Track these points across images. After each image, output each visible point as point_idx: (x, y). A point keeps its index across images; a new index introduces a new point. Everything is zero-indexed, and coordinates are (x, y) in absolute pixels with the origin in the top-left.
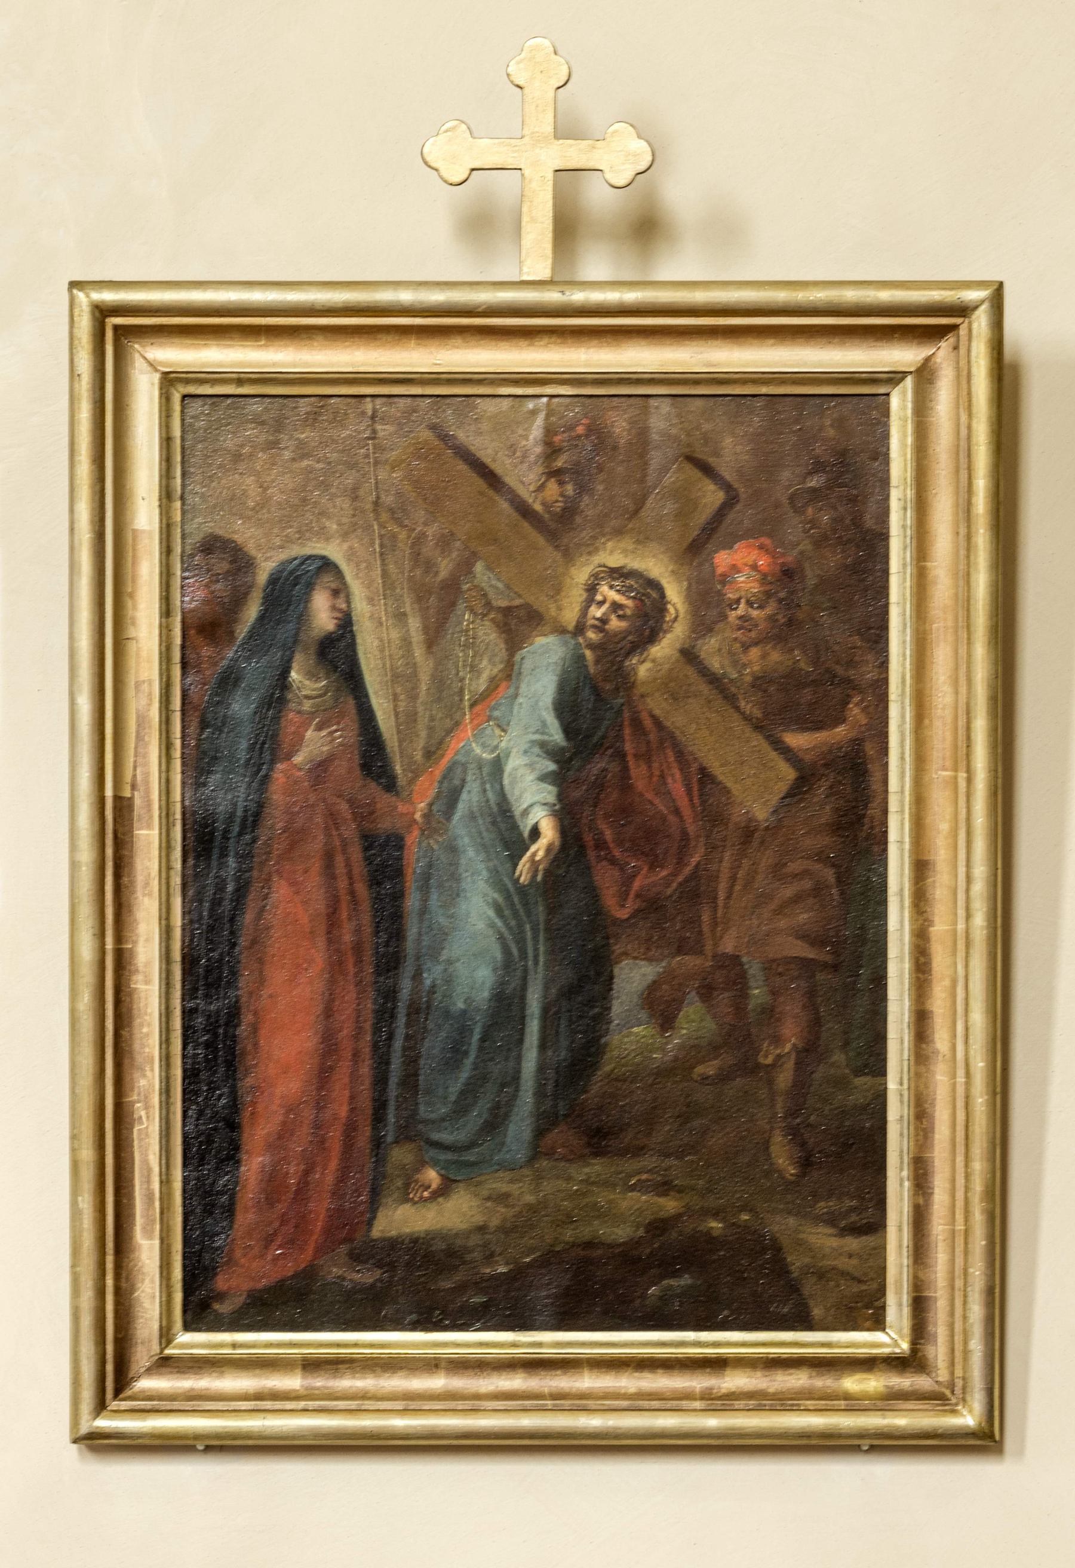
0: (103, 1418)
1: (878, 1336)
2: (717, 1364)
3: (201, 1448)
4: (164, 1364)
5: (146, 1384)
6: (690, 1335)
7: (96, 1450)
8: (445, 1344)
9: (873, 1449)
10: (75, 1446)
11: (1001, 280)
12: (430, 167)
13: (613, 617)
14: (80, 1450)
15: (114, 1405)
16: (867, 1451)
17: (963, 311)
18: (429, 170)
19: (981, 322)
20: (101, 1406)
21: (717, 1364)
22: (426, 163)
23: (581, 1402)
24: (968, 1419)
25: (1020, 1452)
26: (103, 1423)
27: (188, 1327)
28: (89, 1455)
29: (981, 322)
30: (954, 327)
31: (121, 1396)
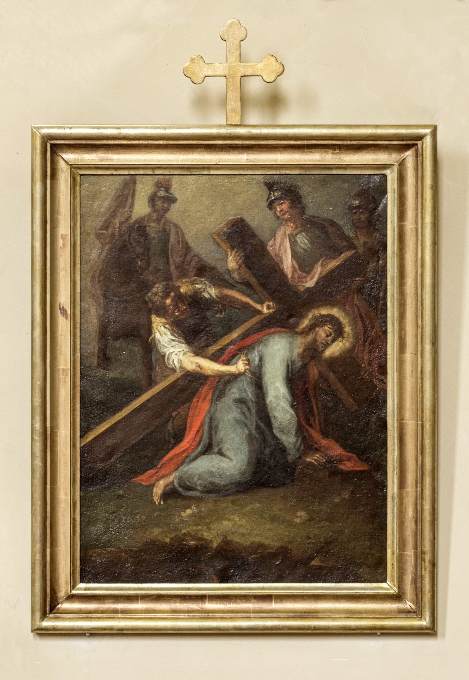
0: (47, 621)
1: (384, 585)
2: (201, 598)
3: (379, 634)
4: (71, 598)
5: (66, 606)
6: (332, 585)
7: (39, 635)
8: (189, 589)
9: (382, 634)
10: (32, 633)
11: (436, 124)
12: (282, 74)
13: (236, 273)
14: (34, 635)
15: (51, 615)
16: (379, 636)
17: (421, 138)
18: (283, 74)
19: (428, 141)
20: (44, 616)
21: (201, 598)
22: (190, 78)
23: (208, 614)
24: (425, 622)
25: (444, 635)
26: (46, 624)
27: (82, 581)
28: (37, 637)
29: (428, 141)
30: (413, 145)
31: (53, 612)
